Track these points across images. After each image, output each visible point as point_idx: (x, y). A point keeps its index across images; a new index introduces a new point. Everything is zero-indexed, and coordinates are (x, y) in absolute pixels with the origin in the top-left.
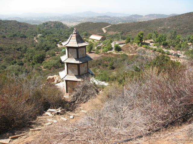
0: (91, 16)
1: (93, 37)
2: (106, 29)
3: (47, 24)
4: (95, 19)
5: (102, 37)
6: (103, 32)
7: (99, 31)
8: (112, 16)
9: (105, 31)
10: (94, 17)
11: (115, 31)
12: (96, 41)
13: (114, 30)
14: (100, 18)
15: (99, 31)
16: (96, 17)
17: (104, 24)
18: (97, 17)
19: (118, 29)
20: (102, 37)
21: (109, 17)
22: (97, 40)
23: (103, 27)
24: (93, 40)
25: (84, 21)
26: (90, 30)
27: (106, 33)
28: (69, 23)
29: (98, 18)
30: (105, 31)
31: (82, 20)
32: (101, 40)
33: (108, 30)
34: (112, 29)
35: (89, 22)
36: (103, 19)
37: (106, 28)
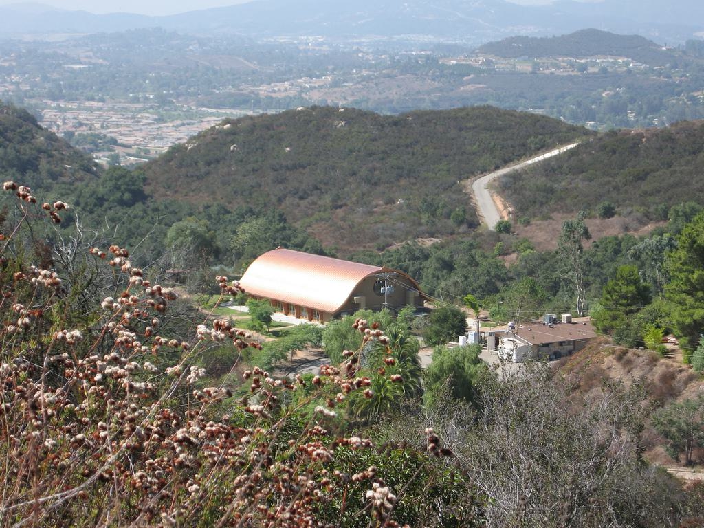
0: (430, 38)
1: (269, 275)
2: (508, 188)
3: (545, 261)
4: (469, 69)
5: (366, 270)
6: (471, 220)
7: (431, 208)
8: (671, 41)
9: (491, 209)
10: (452, 50)
11: (609, 213)
12: (292, 320)
13: (598, 198)
14: (525, 67)
15: (431, 208)
16: (473, 53)
17: (493, 133)
18: (493, 48)
19: (645, 186)
20: (366, 270)
21: (634, 45)
22: (312, 313)
23: (484, 171)
24: (264, 308)
25: (285, 93)
26: (327, 199)
27: (504, 228)
28: (148, 117)
29: (501, 64)
30: (491, 209)
31: (304, 82)
32: (350, 307)
33: (527, 198)
34: (580, 183)
35: (328, 113)
36: (563, 67)
37: (516, 177)
